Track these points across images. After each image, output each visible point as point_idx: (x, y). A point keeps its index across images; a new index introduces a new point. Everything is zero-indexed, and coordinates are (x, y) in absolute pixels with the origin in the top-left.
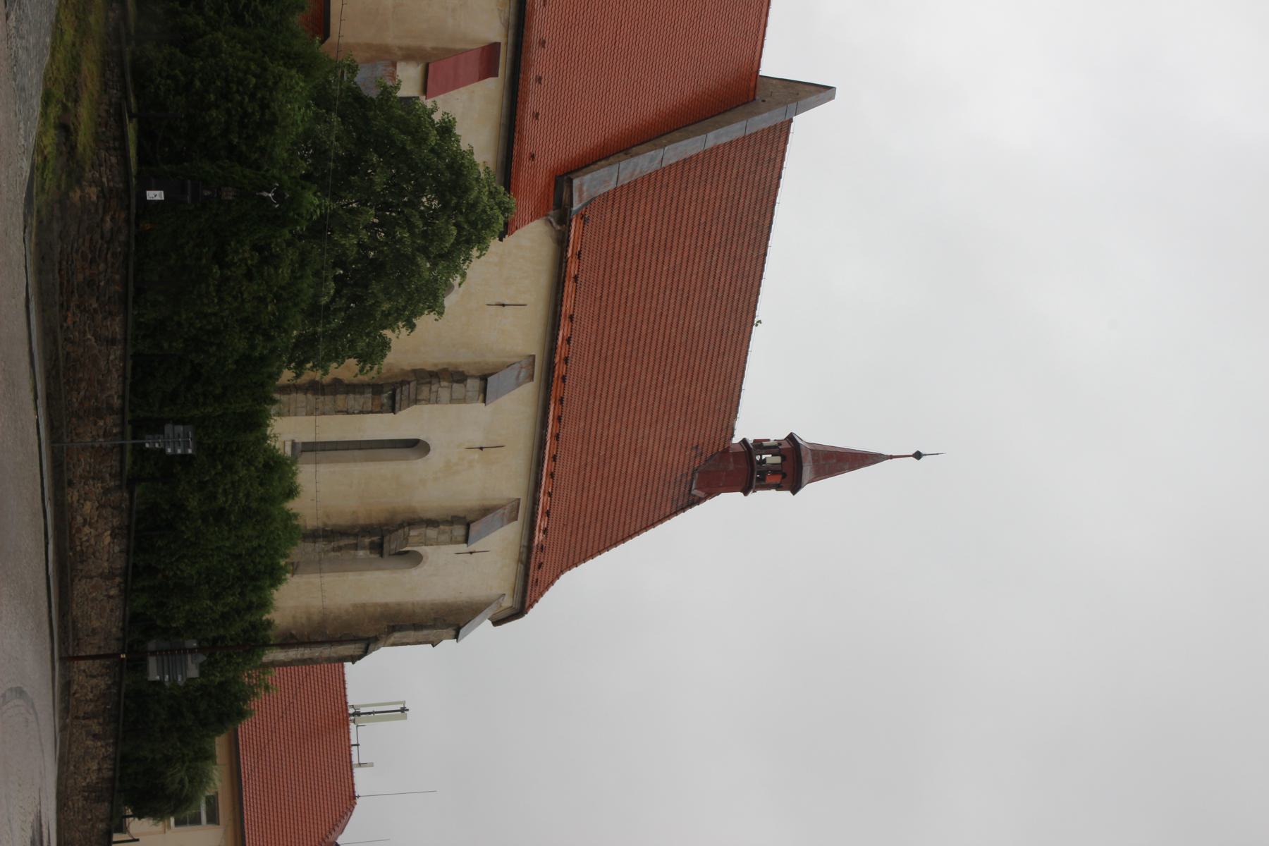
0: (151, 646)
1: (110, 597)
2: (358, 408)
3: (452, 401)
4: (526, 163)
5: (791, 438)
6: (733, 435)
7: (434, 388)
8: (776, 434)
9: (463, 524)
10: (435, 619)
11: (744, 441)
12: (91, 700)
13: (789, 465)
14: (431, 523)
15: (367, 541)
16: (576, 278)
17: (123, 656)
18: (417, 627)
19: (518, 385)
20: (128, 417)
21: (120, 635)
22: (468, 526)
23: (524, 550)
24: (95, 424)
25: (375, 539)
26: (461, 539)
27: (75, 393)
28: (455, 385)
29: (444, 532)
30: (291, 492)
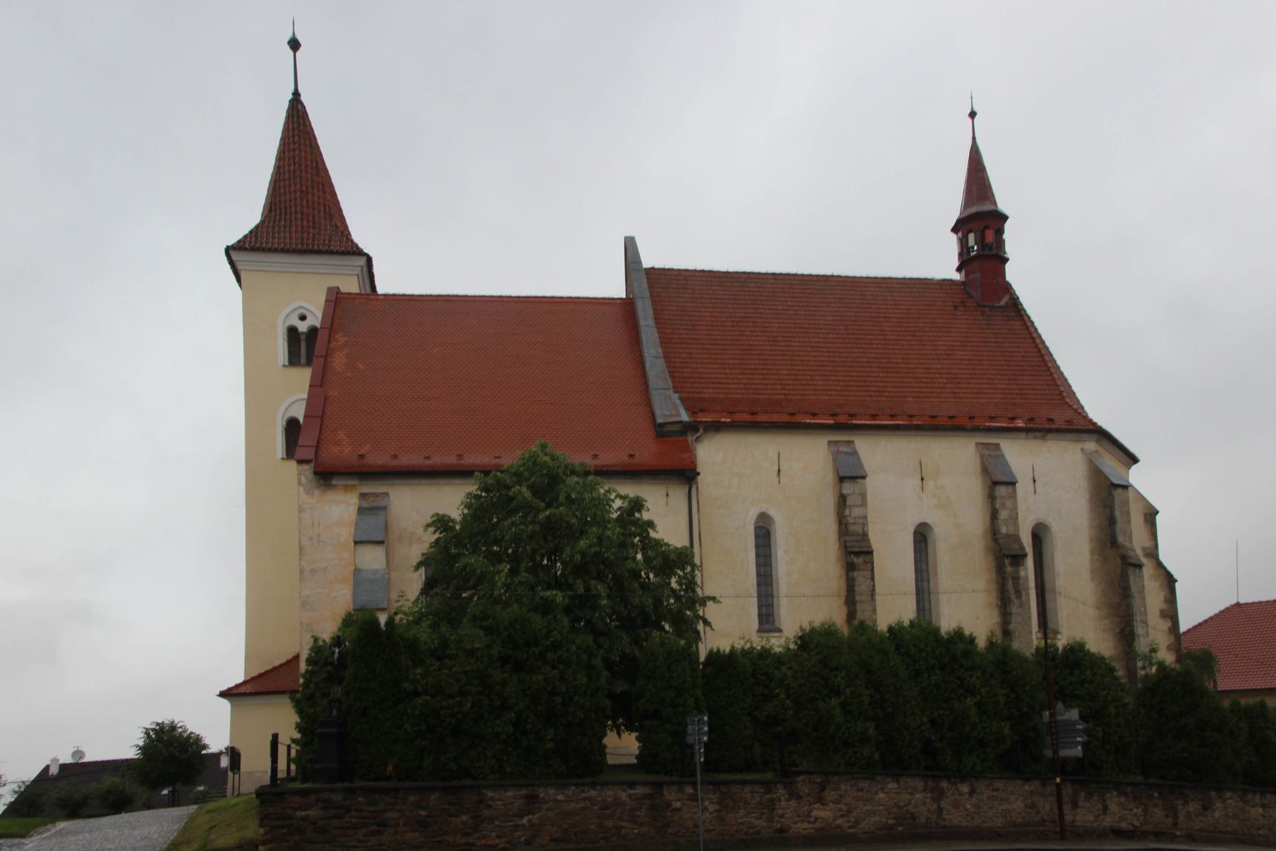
0: (1048, 753)
1: (973, 791)
2: (869, 582)
3: (864, 504)
4: (637, 459)
5: (955, 230)
6: (951, 280)
7: (851, 521)
8: (953, 242)
9: (998, 483)
10: (1105, 507)
11: (959, 270)
12: (1146, 810)
13: (981, 226)
14: (994, 515)
15: (1009, 569)
16: (791, 414)
17: (1058, 780)
18: (1112, 521)
19: (855, 453)
20: (1140, 779)
21: (1037, 783)
22: (996, 483)
23: (1031, 435)
24: (678, 810)
25: (1007, 562)
26: (1010, 489)
27: (623, 831)
28: (848, 503)
29: (1003, 504)
30: (972, 640)
